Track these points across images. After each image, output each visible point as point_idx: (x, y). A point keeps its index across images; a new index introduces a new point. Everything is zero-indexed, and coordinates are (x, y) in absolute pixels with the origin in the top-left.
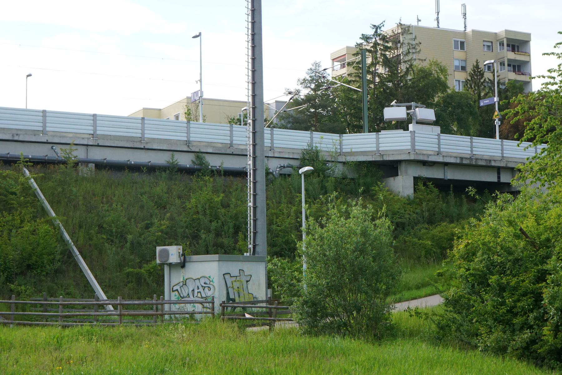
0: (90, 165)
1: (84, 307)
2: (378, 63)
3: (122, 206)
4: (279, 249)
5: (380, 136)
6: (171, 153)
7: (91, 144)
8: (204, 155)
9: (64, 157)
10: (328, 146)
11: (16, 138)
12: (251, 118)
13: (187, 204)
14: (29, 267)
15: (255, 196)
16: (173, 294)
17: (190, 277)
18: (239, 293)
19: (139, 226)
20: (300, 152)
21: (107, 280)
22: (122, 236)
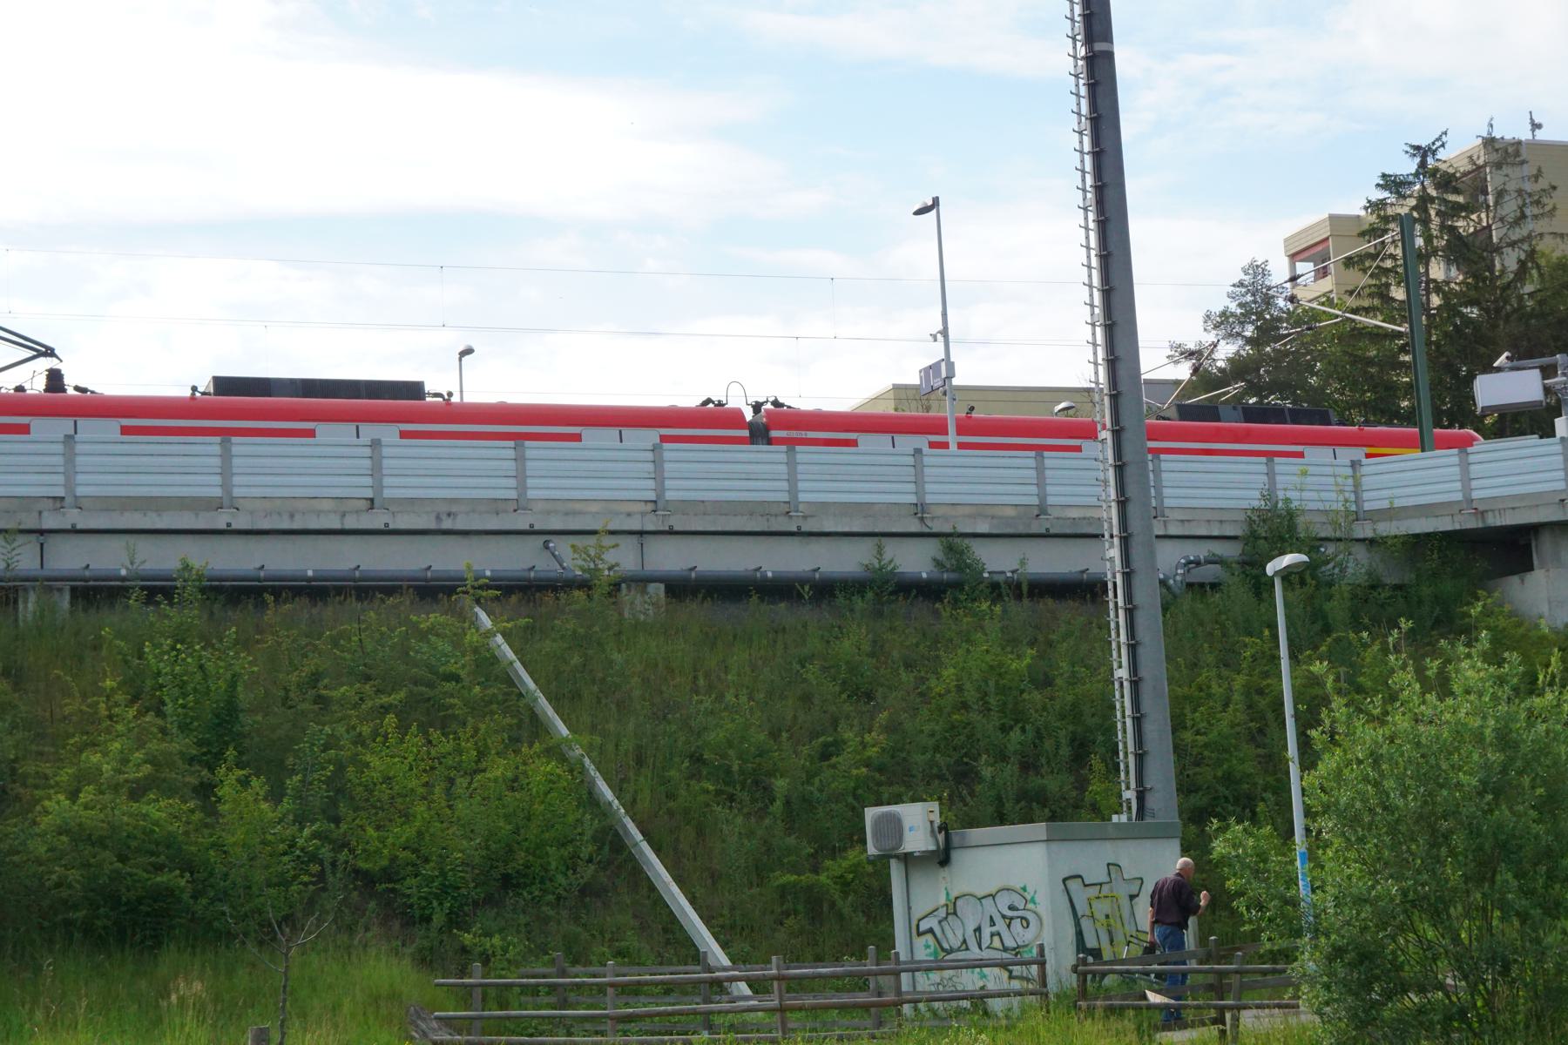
0: (652, 587)
1: (668, 989)
2: (1435, 252)
3: (751, 698)
4: (1205, 800)
5: (1472, 458)
6: (876, 540)
7: (651, 527)
8: (967, 541)
9: (582, 568)
10: (1324, 495)
11: (447, 524)
12: (1109, 425)
13: (933, 682)
14: (506, 881)
15: (1133, 648)
16: (920, 942)
17: (966, 890)
18: (1110, 933)
19: (805, 750)
20: (1242, 517)
21: (726, 912)
22: (756, 783)
